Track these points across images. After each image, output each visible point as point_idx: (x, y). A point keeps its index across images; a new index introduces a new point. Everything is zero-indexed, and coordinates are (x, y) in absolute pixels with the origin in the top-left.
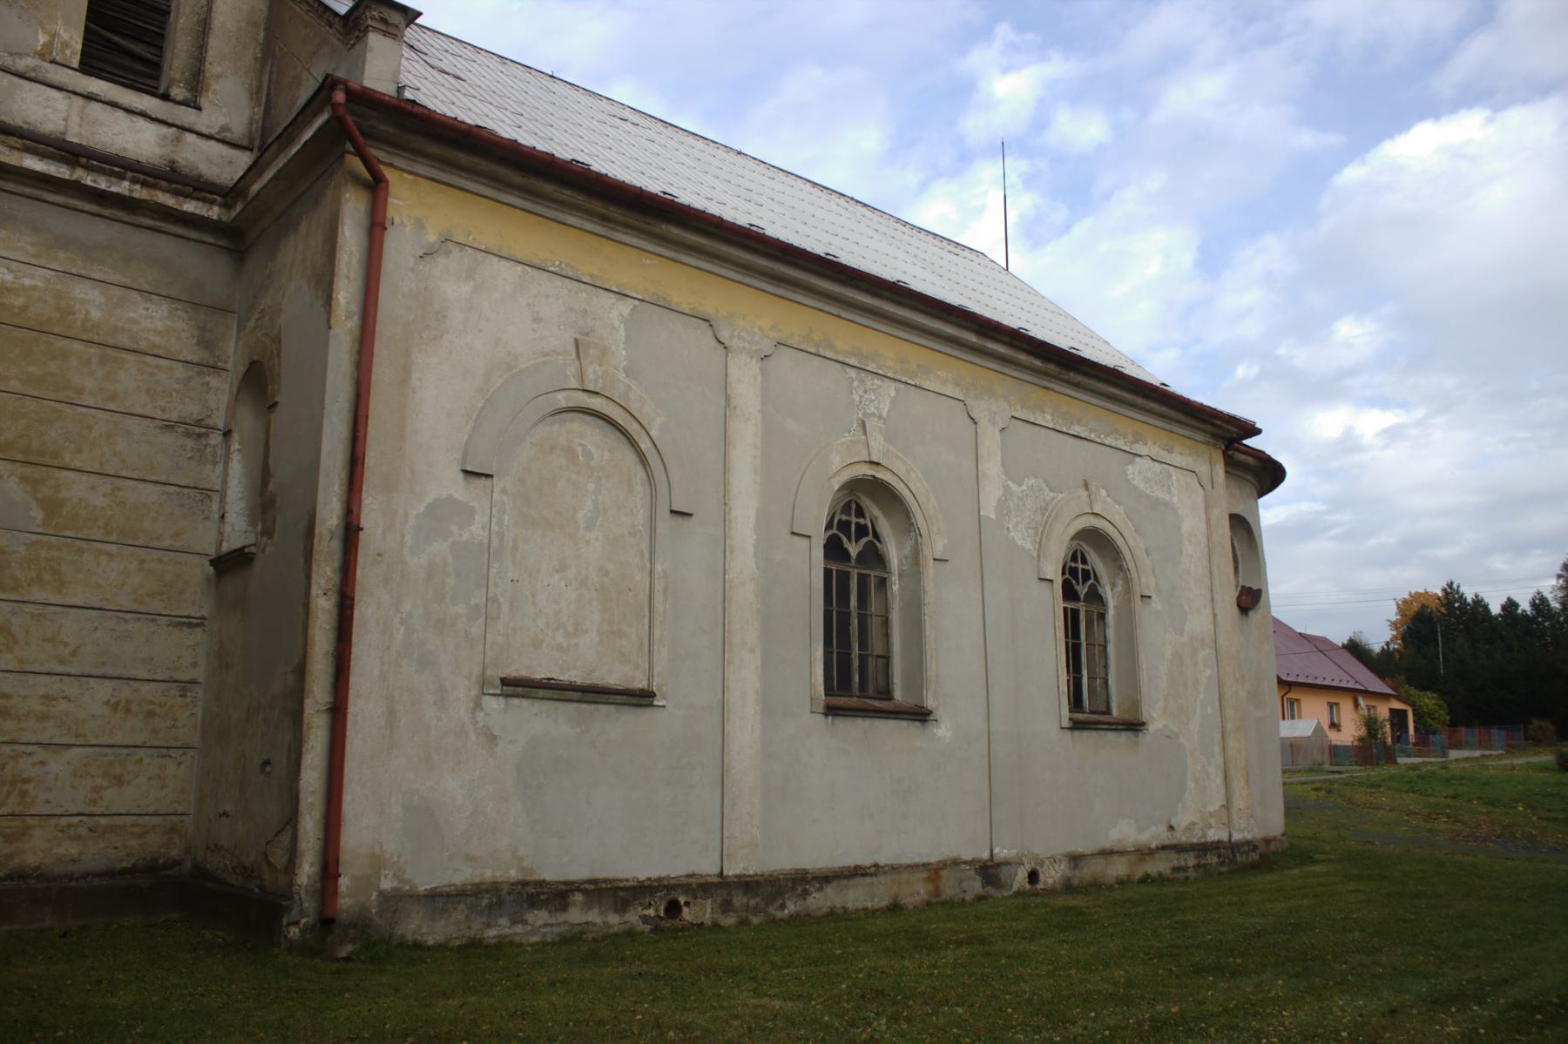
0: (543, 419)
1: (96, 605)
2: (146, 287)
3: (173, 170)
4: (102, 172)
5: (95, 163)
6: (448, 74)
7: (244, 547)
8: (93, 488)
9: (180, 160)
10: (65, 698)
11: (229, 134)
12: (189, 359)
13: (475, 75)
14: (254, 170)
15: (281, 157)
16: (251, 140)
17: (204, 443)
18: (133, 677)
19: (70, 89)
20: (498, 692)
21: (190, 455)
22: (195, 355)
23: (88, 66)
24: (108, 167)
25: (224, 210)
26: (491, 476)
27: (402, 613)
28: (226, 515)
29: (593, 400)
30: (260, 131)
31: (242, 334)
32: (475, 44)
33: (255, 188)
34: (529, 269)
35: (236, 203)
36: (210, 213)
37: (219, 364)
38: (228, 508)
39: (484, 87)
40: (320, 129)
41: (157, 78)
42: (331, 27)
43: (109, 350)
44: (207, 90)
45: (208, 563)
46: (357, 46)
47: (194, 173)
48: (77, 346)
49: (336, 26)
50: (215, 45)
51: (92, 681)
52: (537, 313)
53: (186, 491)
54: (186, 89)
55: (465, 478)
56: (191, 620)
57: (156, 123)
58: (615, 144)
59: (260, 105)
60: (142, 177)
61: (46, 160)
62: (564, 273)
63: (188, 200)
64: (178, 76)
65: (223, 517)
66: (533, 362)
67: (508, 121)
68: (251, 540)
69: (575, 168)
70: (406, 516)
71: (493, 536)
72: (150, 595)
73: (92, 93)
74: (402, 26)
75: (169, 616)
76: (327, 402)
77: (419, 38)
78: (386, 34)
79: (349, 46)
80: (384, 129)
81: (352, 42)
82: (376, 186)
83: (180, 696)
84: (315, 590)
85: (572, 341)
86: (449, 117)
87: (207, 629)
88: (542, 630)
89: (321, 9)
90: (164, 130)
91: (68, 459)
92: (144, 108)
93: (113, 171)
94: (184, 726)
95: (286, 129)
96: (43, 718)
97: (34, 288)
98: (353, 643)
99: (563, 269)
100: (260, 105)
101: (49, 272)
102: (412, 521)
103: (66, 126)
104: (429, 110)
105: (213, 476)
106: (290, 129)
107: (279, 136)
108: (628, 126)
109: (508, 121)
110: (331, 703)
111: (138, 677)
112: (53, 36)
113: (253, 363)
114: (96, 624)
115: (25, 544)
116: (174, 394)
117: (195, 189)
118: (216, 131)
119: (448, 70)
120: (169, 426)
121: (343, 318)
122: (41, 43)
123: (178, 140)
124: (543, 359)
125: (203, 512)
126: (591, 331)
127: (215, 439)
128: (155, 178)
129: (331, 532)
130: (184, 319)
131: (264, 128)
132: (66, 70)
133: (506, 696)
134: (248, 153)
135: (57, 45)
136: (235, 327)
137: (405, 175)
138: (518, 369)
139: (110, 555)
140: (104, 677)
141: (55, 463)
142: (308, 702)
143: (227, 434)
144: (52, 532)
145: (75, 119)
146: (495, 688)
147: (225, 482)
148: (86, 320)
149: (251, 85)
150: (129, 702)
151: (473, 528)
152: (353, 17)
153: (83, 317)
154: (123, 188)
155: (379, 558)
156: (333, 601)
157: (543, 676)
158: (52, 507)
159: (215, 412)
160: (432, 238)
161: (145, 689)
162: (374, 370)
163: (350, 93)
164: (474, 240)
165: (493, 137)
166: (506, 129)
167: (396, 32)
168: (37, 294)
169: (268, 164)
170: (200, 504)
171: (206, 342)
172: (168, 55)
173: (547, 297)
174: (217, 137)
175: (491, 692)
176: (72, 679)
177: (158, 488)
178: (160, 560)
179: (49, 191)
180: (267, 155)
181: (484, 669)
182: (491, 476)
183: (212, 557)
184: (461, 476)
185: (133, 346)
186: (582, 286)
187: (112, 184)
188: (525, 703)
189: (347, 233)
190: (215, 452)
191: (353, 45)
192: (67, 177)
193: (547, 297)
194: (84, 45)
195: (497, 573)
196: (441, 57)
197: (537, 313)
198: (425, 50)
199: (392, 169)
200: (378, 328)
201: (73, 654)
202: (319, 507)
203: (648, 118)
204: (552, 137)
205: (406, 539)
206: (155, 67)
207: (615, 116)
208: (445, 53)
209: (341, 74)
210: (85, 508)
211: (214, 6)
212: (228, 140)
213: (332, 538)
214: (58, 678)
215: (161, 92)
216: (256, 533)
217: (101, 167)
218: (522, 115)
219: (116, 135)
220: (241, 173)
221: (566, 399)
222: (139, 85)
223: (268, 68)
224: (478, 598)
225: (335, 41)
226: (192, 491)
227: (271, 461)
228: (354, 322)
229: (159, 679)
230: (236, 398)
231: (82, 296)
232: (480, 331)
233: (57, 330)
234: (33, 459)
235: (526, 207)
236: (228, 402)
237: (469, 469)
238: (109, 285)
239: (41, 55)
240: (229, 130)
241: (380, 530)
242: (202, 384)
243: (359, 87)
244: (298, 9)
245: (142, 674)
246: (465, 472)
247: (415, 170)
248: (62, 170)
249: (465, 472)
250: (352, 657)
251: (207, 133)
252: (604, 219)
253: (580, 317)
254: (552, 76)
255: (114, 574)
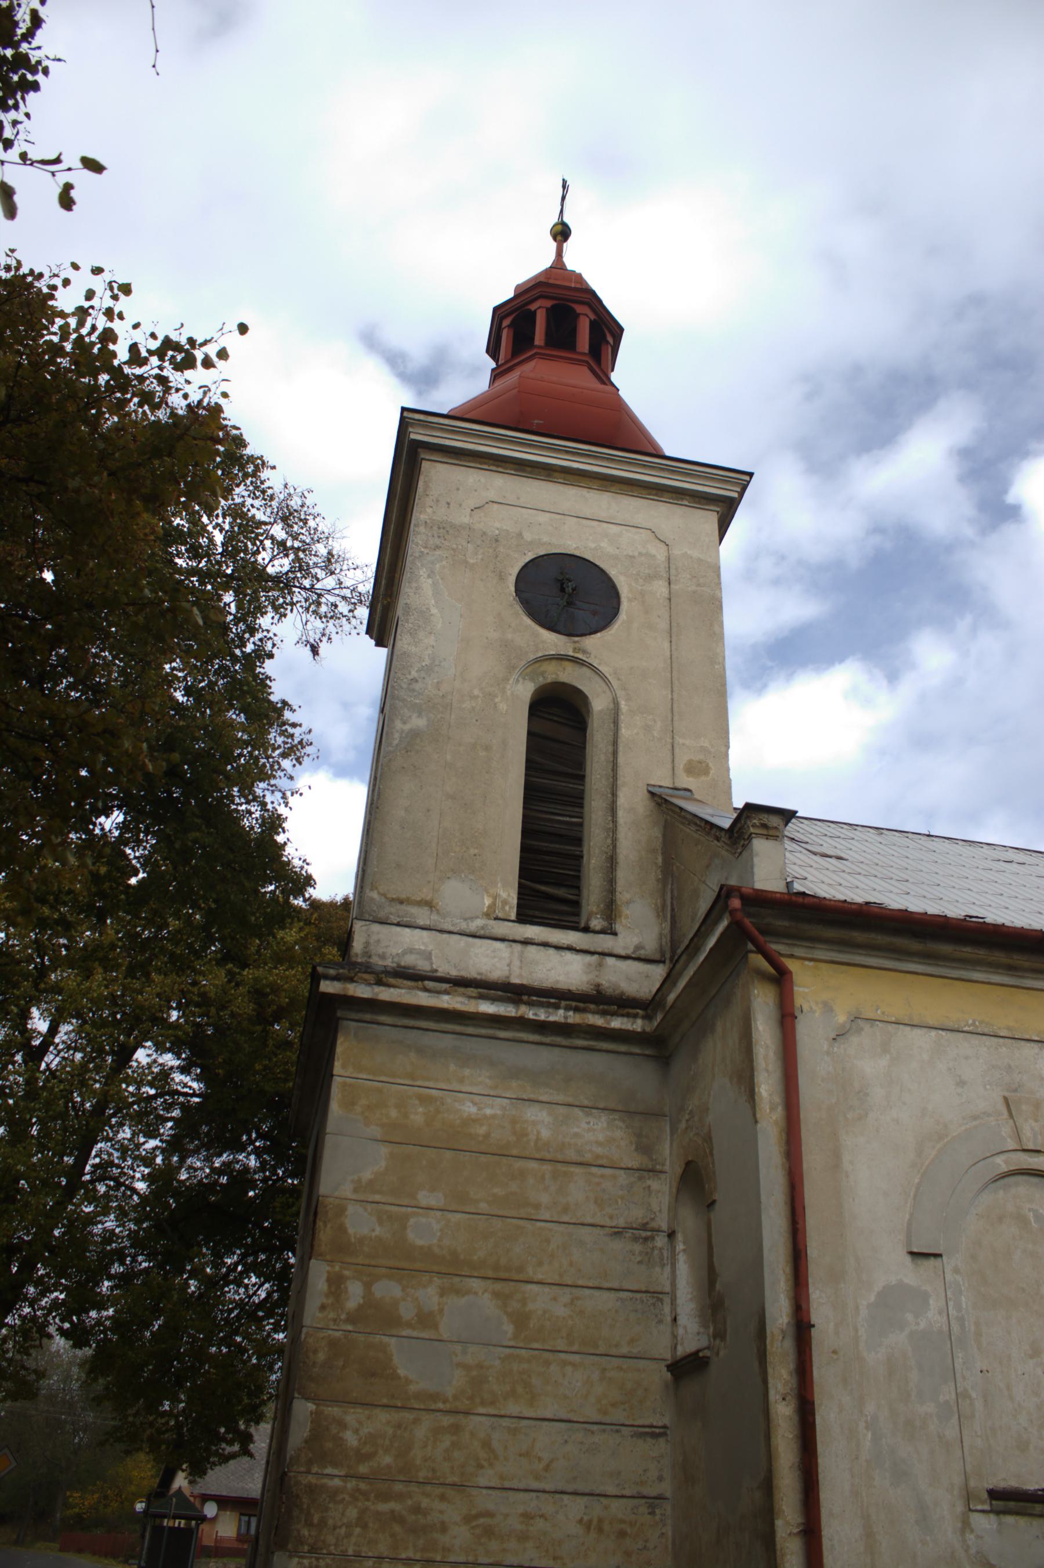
0: (985, 1186)
1: (564, 1416)
2: (586, 1103)
3: (599, 992)
4: (541, 1005)
5: (535, 998)
6: (830, 857)
7: (698, 1351)
8: (555, 1299)
9: (604, 983)
10: (542, 1516)
11: (642, 952)
12: (630, 1166)
13: (855, 851)
14: (669, 980)
15: (691, 965)
16: (663, 954)
17: (651, 1246)
18: (603, 1493)
19: (511, 939)
20: (987, 1507)
21: (639, 1259)
22: (634, 1160)
23: (524, 917)
24: (545, 1000)
25: (647, 1022)
26: (939, 1255)
27: (866, 1416)
28: (678, 1318)
29: (1036, 1160)
30: (669, 944)
31: (675, 1136)
32: (851, 823)
33: (672, 997)
34: (943, 1033)
35: (656, 1014)
36: (634, 1026)
37: (658, 1167)
38: (679, 1310)
39: (866, 861)
40: (722, 934)
41: (578, 914)
42: (718, 840)
43: (559, 1166)
44: (620, 917)
45: (666, 1369)
46: (744, 853)
47: (617, 992)
48: (533, 1165)
49: (723, 839)
50: (622, 875)
51: (565, 1497)
52: (960, 1076)
53: (638, 1296)
54: (603, 919)
55: (913, 1260)
56: (653, 1429)
57: (581, 954)
58: (1006, 890)
59: (666, 921)
60: (574, 1004)
61: (496, 1003)
62: (979, 1030)
63: (614, 1018)
64: (595, 909)
65: (675, 1320)
66: (963, 1128)
67: (895, 890)
68: (704, 1342)
69: (969, 924)
70: (857, 1308)
71: (953, 1322)
72: (614, 1405)
73: (528, 938)
74: (781, 827)
75: (632, 1426)
76: (763, 1198)
77: (798, 829)
78: (768, 837)
79: (737, 855)
80: (780, 924)
81: (739, 851)
82: (781, 979)
83: (649, 1513)
84: (773, 1396)
85: (1001, 1101)
86: (839, 901)
87: (669, 1438)
88: (1026, 1429)
89: (708, 827)
90: (588, 958)
91: (531, 1273)
92: (569, 943)
93: (549, 1002)
94: (655, 1547)
95: (692, 940)
96: (523, 1538)
97: (494, 1117)
98: (819, 1453)
99: (977, 1027)
100: (666, 921)
101: (505, 1100)
102: (864, 1312)
103: (510, 971)
104: (818, 898)
105: (661, 1278)
106: (695, 940)
107: (687, 947)
108: (1014, 867)
109: (895, 890)
110: (804, 1524)
111: (608, 1493)
112: (495, 897)
113: (688, 1164)
114: (566, 1437)
115: (500, 1358)
116: (620, 1201)
117: (619, 1007)
118: (632, 950)
119: (829, 853)
120: (617, 1233)
121: (768, 1111)
122: (487, 905)
123: (600, 965)
124: (975, 1123)
125: (656, 1316)
126: (1019, 1086)
127: (661, 1241)
128: (584, 1002)
129: (782, 1331)
130: (621, 1128)
131: (672, 940)
132: (506, 923)
133: (998, 1513)
134: (661, 965)
135: (499, 903)
136: (668, 1128)
137: (807, 963)
138: (949, 1138)
139: (573, 1365)
140: (575, 1493)
141: (521, 1277)
142: (779, 1523)
143: (671, 1235)
144: (521, 1345)
145: (516, 963)
146: (983, 1503)
147: (673, 1284)
148: (538, 1139)
149: (656, 905)
150: (600, 1520)
151: (930, 1314)
152: (736, 829)
153: (535, 1137)
154: (558, 1016)
155: (835, 1357)
156: (793, 1406)
157: (1037, 1487)
158: (521, 1320)
159: (657, 1214)
160: (842, 1018)
161: (615, 1505)
162: (805, 1158)
163: (744, 898)
164: (883, 1013)
165: (884, 911)
166: (895, 901)
167: (777, 834)
168: (497, 1122)
169: (680, 974)
170: (652, 1307)
171: (644, 1148)
172: (585, 893)
173: (967, 1058)
174: (633, 956)
175: (979, 1507)
176: (547, 1495)
177: (613, 1295)
178: (620, 1368)
179: (500, 1029)
180: (678, 966)
181: (966, 1480)
182: (939, 1255)
183: (669, 1362)
184: (908, 1259)
185: (580, 1159)
186: (1001, 1040)
187: (550, 1014)
188: (1022, 1522)
189: (761, 1028)
190: (662, 1254)
191: (741, 853)
192: (513, 1014)
193: (967, 1058)
194: (519, 899)
195: (964, 1363)
196: (821, 842)
197: (960, 1076)
198: (806, 839)
199: (794, 960)
200: (802, 1116)
201: (547, 1468)
202: (767, 1306)
203: (1034, 854)
204: (941, 896)
205: (860, 1333)
206: (576, 904)
207: (999, 860)
208: (824, 838)
209: (733, 882)
210: (549, 1320)
211: (618, 844)
212: (643, 957)
213: (783, 1338)
214: (534, 1494)
215: (582, 925)
216: (708, 1335)
217: (540, 1002)
218: (907, 881)
219: (549, 970)
220: (658, 986)
221: (1006, 1162)
222: (564, 923)
223: (670, 886)
224: (947, 1394)
225: (724, 853)
226: (644, 1295)
227: (715, 1260)
228: (779, 1113)
229: (628, 1495)
230: (677, 1198)
231: (533, 1118)
232: (904, 1103)
233: (514, 1152)
234: (503, 1275)
235: (929, 972)
236: (669, 1203)
237: (915, 1250)
238: (554, 1106)
239: (487, 915)
240: (643, 948)
241: (832, 1325)
242: (644, 1188)
243: (751, 891)
244: (688, 830)
245: (611, 1490)
246: (912, 1253)
247: (815, 956)
248: (509, 1009)
249: (912, 1253)
250: (820, 1470)
251: (624, 954)
252: (1011, 969)
253: (1005, 1073)
254: (929, 836)
255: (579, 1384)
